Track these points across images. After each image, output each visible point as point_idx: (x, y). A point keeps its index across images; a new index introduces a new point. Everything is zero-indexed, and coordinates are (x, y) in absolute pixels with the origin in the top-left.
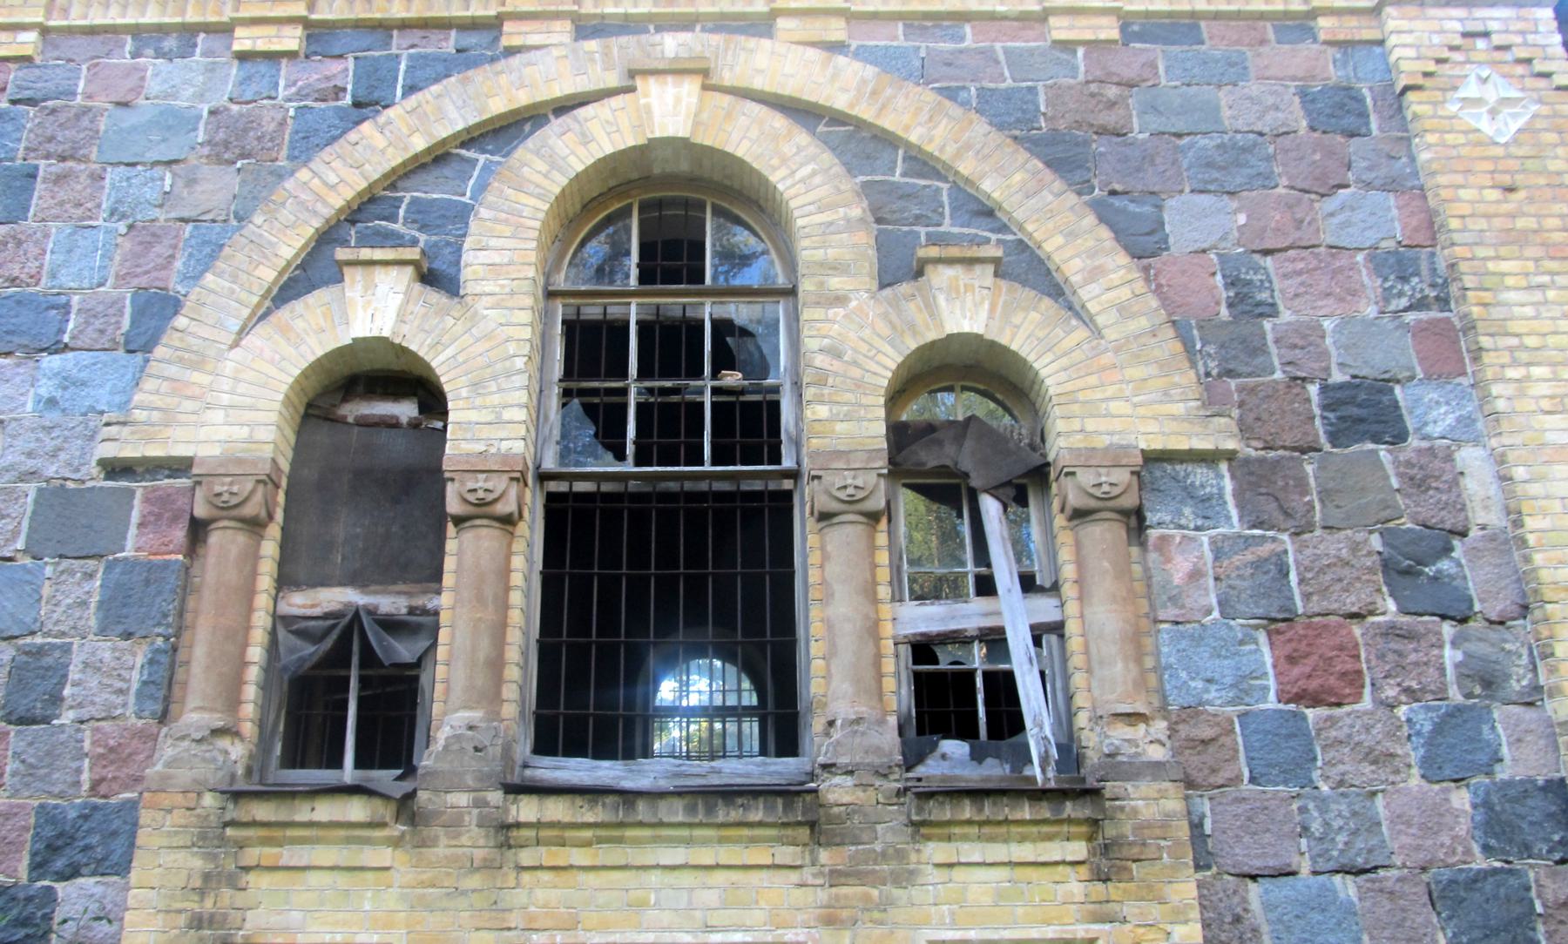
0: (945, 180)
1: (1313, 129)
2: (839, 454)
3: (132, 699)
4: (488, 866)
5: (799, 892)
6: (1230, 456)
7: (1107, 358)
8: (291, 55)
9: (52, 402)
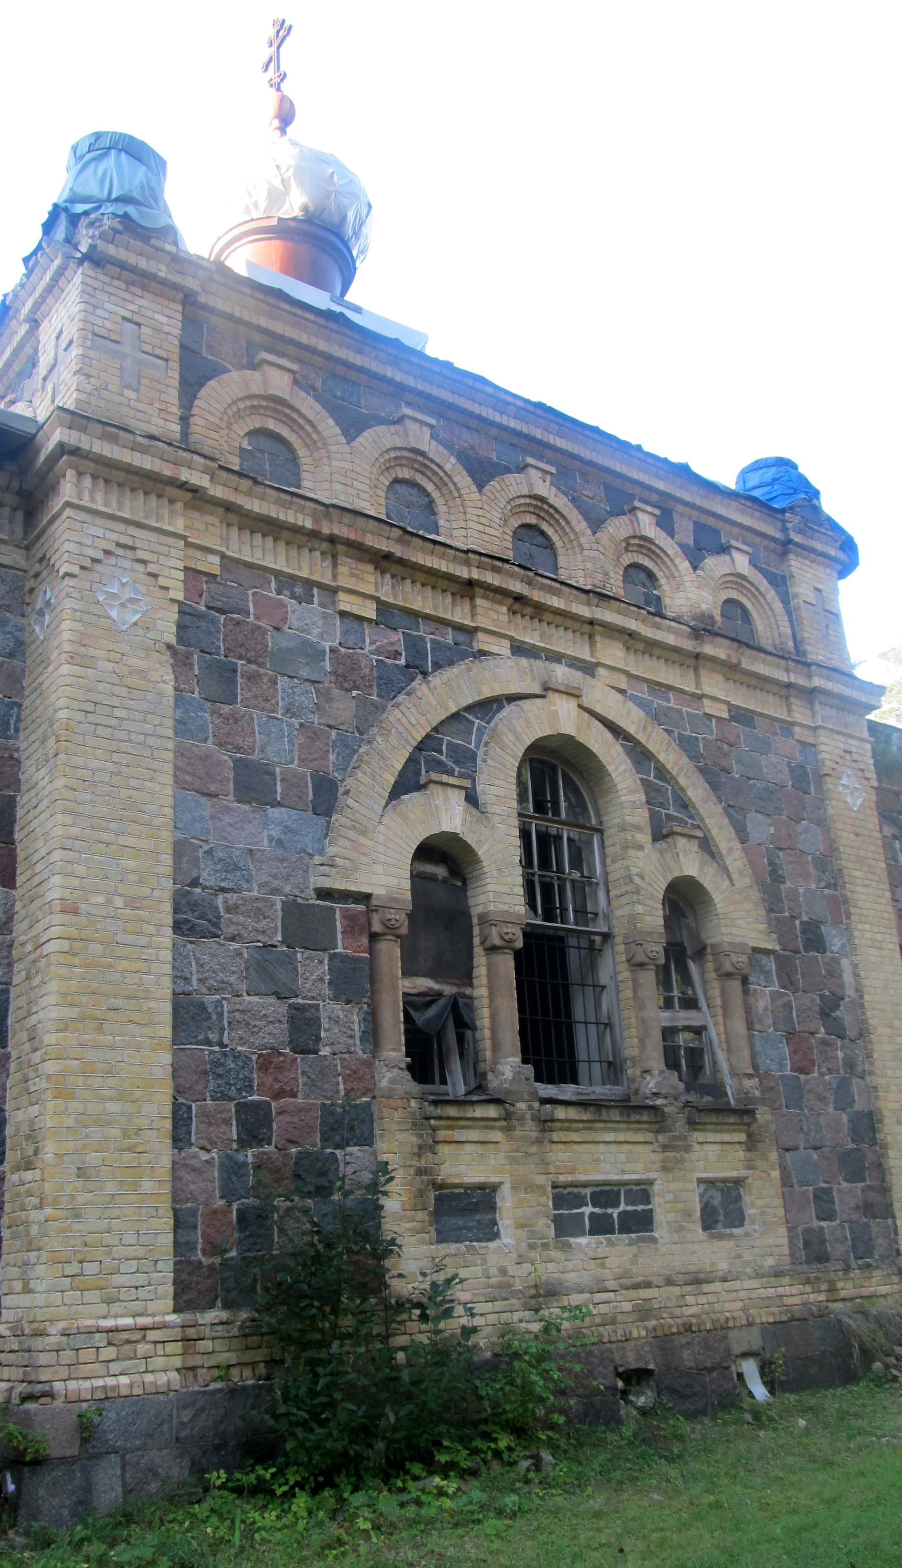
0: (669, 783)
1: (793, 786)
2: (649, 933)
3: (358, 1042)
4: (539, 1141)
5: (653, 1155)
6: (773, 952)
7: (737, 897)
8: (370, 621)
9: (280, 842)
